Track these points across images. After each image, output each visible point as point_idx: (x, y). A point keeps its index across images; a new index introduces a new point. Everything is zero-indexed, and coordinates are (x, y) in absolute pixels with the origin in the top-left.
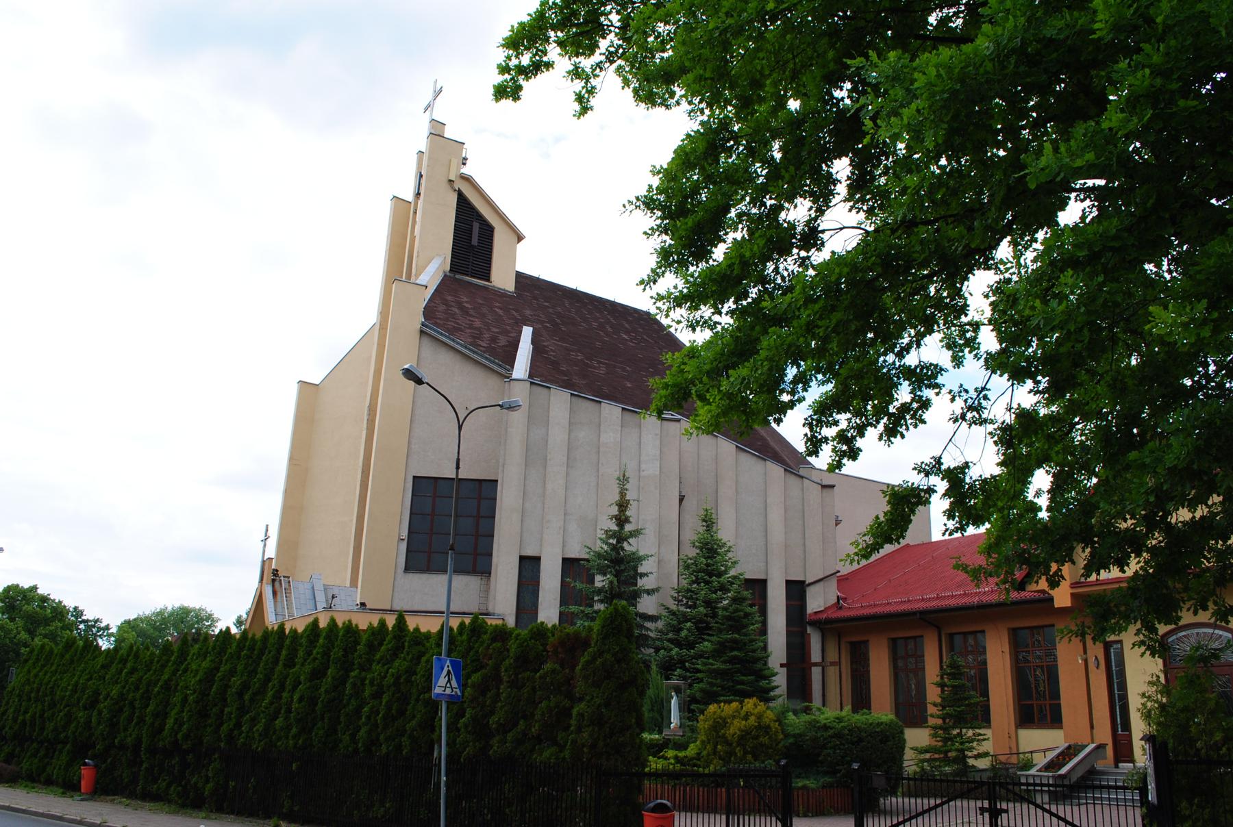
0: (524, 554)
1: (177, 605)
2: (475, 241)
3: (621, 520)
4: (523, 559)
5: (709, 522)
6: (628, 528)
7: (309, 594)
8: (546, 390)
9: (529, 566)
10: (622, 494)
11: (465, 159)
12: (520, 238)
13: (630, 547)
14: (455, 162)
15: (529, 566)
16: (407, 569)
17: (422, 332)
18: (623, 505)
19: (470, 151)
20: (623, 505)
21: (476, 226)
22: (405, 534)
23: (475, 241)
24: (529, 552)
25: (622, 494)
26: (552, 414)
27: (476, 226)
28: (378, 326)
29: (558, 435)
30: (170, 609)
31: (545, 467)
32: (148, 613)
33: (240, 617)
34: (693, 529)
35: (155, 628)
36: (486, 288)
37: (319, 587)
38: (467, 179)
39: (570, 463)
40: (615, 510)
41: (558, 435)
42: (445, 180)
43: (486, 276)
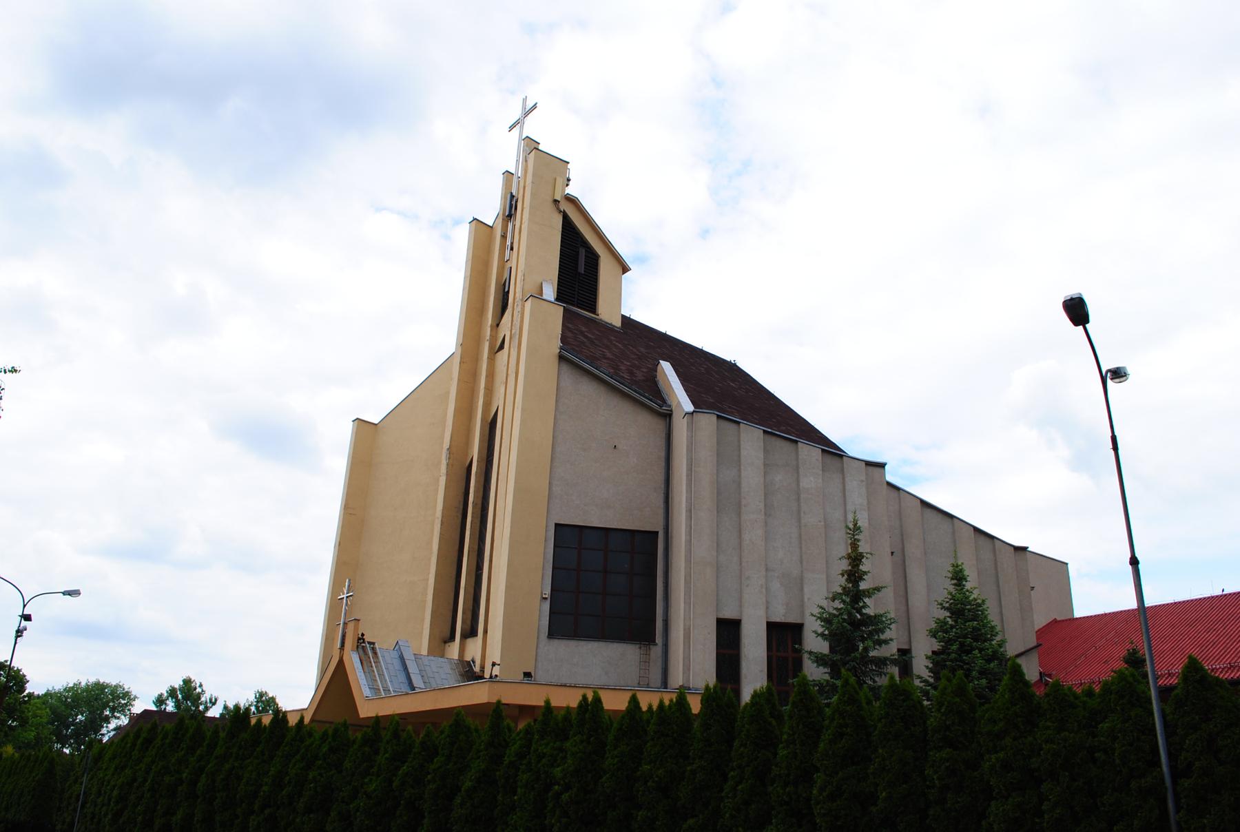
0: (721, 616)
1: (92, 680)
2: (581, 269)
3: (854, 575)
4: (720, 622)
5: (958, 577)
6: (863, 586)
7: (397, 664)
8: (733, 426)
9: (729, 631)
10: (854, 545)
11: (569, 180)
12: (625, 269)
13: (871, 607)
14: (560, 182)
15: (729, 631)
16: (552, 635)
17: (561, 358)
18: (855, 559)
19: (574, 172)
20: (855, 559)
21: (582, 252)
22: (547, 592)
23: (581, 269)
24: (728, 614)
25: (854, 545)
26: (744, 453)
27: (582, 252)
28: (457, 360)
29: (752, 477)
30: (83, 684)
31: (739, 515)
32: (57, 688)
33: (161, 695)
34: (945, 588)
35: (65, 704)
36: (594, 321)
37: (408, 656)
38: (572, 200)
39: (768, 510)
40: (845, 565)
41: (752, 477)
42: (550, 200)
43: (593, 307)
